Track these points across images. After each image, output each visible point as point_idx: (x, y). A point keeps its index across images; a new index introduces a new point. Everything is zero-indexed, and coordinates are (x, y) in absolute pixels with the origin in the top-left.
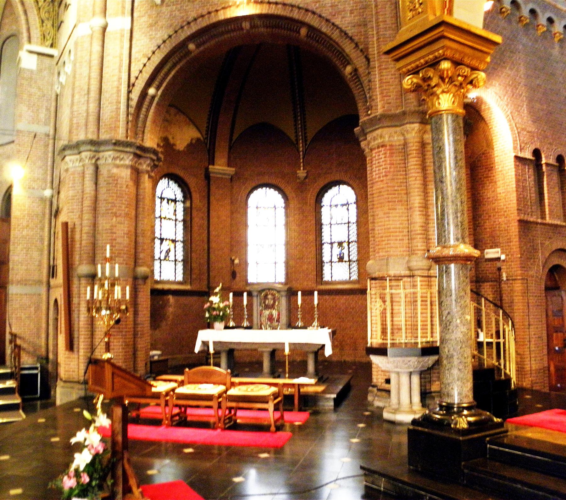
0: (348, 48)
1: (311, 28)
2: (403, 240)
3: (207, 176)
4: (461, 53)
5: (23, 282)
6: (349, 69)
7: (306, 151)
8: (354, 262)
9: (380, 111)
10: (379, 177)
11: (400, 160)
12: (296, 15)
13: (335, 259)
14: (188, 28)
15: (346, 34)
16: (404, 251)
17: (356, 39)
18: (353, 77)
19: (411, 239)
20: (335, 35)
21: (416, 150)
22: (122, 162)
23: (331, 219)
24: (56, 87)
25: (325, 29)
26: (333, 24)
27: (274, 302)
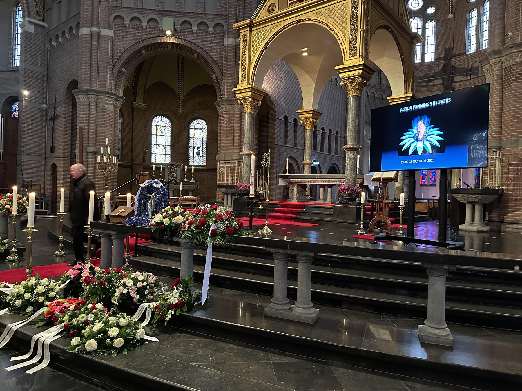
0: (215, 68)
1: (199, 54)
3: (132, 108)
4: (255, 96)
5: (29, 154)
6: (214, 76)
7: (183, 100)
8: (205, 156)
9: (226, 97)
10: (224, 124)
13: (195, 154)
14: (142, 42)
15: (214, 60)
18: (216, 79)
20: (210, 60)
21: (238, 115)
22: (109, 102)
23: (194, 135)
24: (47, 46)
27: (175, 170)
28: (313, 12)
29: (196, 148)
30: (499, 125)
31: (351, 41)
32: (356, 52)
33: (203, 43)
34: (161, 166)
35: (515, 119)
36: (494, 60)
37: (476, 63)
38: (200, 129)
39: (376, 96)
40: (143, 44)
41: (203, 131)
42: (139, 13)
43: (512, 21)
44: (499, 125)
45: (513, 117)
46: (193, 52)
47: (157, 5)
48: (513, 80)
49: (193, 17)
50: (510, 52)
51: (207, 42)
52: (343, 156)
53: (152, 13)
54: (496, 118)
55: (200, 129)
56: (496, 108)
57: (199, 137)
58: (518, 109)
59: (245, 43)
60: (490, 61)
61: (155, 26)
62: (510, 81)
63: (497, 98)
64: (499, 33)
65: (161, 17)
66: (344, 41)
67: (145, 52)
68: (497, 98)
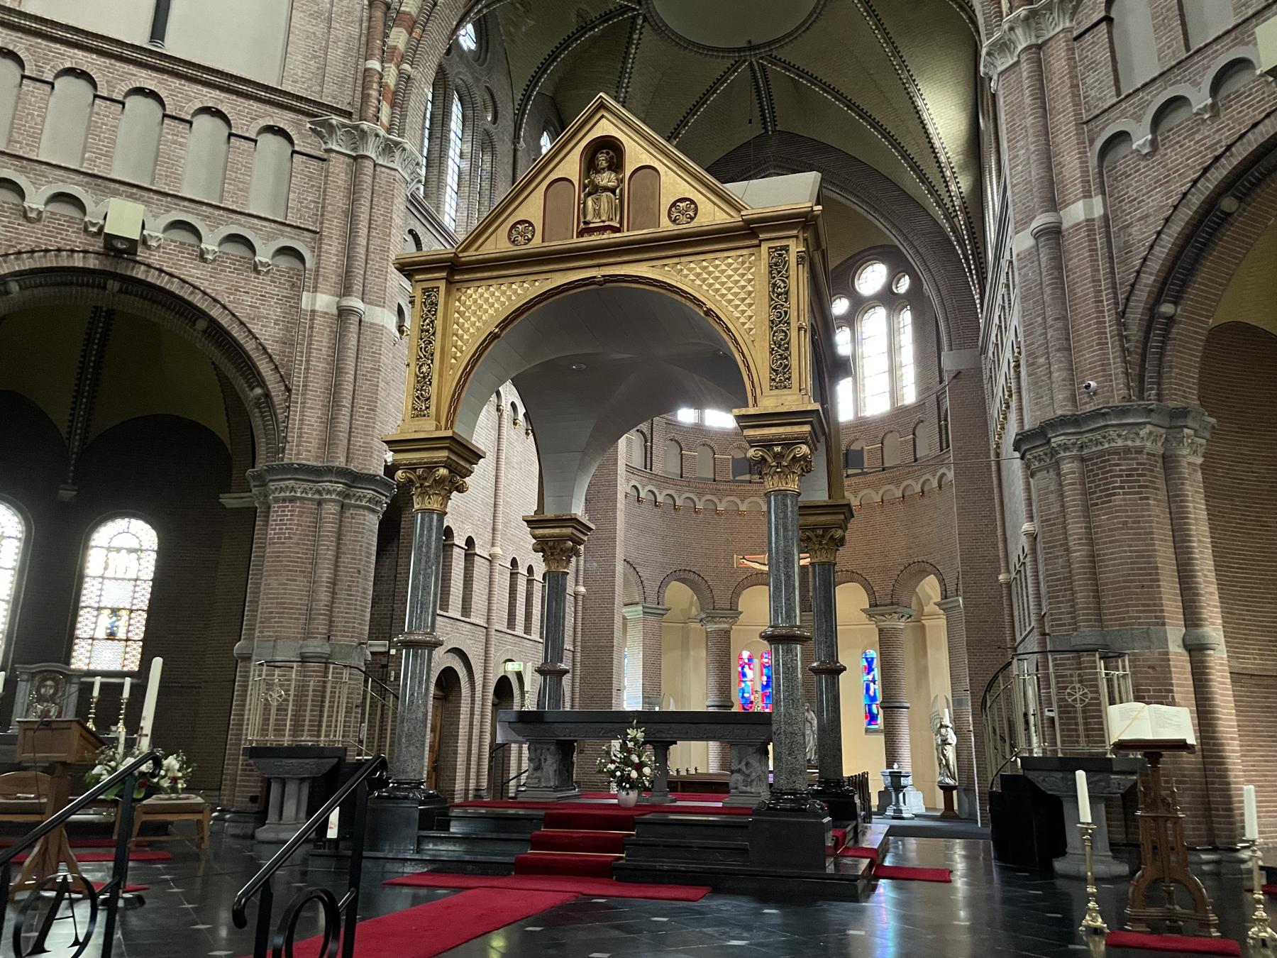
0: (265, 368)
2: (299, 619)
11: (310, 522)
12: (197, 300)
13: (101, 633)
15: (264, 349)
16: (298, 633)
17: (276, 358)
19: (310, 619)
20: (250, 346)
23: (106, 569)
25: (236, 332)
26: (250, 332)
28: (654, 263)
29: (109, 611)
30: (1093, 591)
31: (773, 349)
32: (789, 379)
33: (231, 294)
34: (128, 681)
35: (1135, 581)
36: (1063, 437)
37: (856, 443)
38: (130, 551)
39: (660, 499)
40: (18, 265)
41: (139, 559)
42: (23, 170)
43: (1093, 356)
44: (1093, 591)
45: (1129, 575)
46: (194, 314)
47: (89, 159)
48: (1114, 488)
49: (208, 217)
50: (1103, 424)
51: (248, 293)
52: (572, 649)
53: (69, 178)
54: (1085, 573)
55: (130, 551)
56: (1079, 551)
57: (122, 576)
58: (1137, 557)
59: (429, 311)
60: (1053, 440)
61: (71, 218)
62: (1108, 489)
63: (1081, 528)
64: (1063, 380)
65: (96, 195)
66: (751, 347)
67: (17, 288)
68: (1081, 528)
